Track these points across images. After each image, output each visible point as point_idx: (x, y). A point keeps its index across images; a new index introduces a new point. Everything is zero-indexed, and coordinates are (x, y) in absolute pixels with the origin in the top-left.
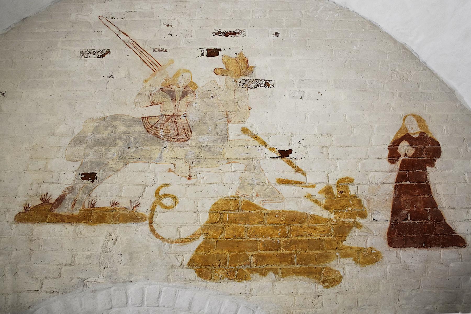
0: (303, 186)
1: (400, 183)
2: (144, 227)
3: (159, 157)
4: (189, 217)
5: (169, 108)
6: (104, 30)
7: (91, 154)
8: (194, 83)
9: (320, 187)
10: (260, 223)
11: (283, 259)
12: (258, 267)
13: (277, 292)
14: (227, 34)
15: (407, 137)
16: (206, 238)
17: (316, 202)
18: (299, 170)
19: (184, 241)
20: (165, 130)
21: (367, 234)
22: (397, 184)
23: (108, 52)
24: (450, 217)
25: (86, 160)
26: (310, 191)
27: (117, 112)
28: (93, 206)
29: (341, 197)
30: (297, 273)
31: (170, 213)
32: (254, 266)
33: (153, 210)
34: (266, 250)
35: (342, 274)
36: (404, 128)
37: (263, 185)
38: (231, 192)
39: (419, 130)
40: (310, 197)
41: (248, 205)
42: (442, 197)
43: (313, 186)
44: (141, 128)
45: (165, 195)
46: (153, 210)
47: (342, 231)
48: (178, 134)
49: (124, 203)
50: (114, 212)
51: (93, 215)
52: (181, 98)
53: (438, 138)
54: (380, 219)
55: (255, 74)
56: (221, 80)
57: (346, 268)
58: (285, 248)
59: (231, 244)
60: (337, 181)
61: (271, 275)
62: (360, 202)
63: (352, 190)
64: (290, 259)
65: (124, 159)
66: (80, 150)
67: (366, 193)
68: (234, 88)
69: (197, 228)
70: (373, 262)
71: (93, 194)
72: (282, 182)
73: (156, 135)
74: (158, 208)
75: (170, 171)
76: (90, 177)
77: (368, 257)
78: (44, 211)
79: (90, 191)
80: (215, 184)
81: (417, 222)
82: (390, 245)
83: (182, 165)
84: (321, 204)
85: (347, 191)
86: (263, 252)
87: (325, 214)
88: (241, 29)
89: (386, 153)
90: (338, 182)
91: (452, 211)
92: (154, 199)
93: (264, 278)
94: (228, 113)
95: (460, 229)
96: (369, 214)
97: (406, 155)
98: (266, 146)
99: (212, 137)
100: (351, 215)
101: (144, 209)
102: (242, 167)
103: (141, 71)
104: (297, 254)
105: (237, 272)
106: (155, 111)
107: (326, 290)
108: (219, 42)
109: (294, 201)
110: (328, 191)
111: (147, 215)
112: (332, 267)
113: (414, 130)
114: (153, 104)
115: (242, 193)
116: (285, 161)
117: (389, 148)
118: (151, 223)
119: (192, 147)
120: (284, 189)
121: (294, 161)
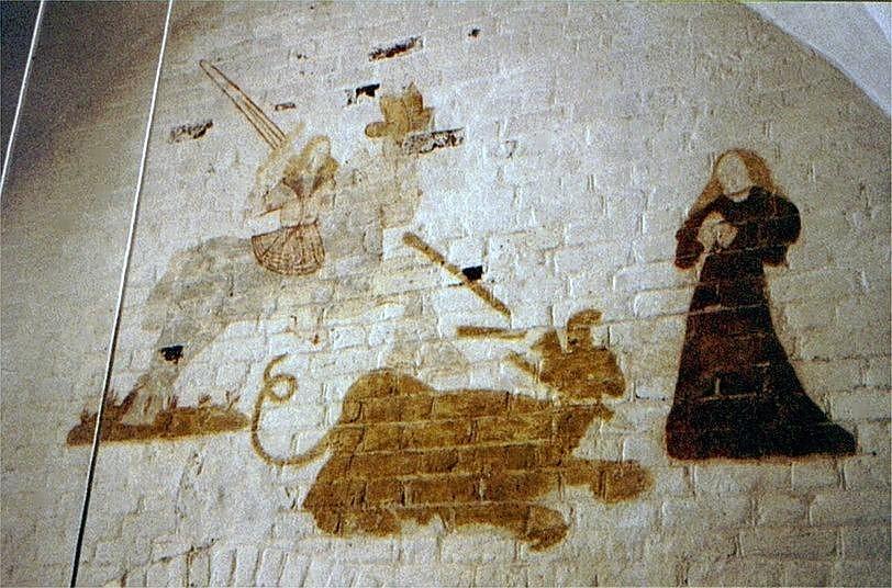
0: (504, 337)
1: (700, 312)
2: (243, 437)
3: (273, 306)
4: (304, 423)
5: (294, 211)
6: (206, 84)
7: (178, 316)
8: (333, 160)
9: (535, 336)
10: (423, 416)
11: (459, 488)
12: (415, 506)
13: (445, 555)
14: (390, 54)
15: (720, 204)
16: (335, 453)
17: (526, 366)
18: (499, 306)
19: (300, 461)
20: (281, 258)
21: (622, 431)
22: (693, 314)
23: (210, 125)
24: (815, 379)
25: (170, 325)
26: (515, 345)
27: (216, 233)
28: (174, 405)
29: (577, 358)
30: (480, 517)
31: (284, 408)
32: (409, 504)
33: (258, 405)
34: (430, 471)
35: (567, 520)
36: (716, 183)
37: (435, 341)
38: (379, 361)
39: (749, 184)
40: (515, 357)
41: (410, 383)
42: (799, 334)
43: (522, 336)
44: (249, 257)
45: (279, 377)
46: (258, 405)
47: (573, 424)
48: (304, 260)
49: (218, 398)
50: (203, 412)
51: (175, 423)
52: (312, 192)
53: (794, 194)
54: (649, 398)
55: (433, 123)
56: (375, 146)
57: (575, 504)
58: (465, 465)
59: (374, 464)
60: (566, 321)
61: (437, 522)
62: (612, 360)
63: (597, 335)
64: (470, 490)
65: (222, 317)
66: (163, 308)
67: (627, 340)
68: (395, 158)
69: (323, 432)
70: (633, 493)
71: (176, 385)
72: (465, 331)
73: (270, 267)
74: (266, 403)
75: (288, 330)
76: (173, 353)
77: (621, 482)
78: (109, 422)
79: (172, 379)
80: (362, 342)
81: (743, 397)
82: (671, 453)
83: (307, 318)
84: (534, 372)
85: (587, 340)
86: (426, 476)
87: (541, 391)
88: (414, 37)
89: (672, 247)
90: (570, 321)
91: (823, 366)
92: (262, 385)
93: (423, 529)
94: (384, 209)
95: (841, 409)
96: (630, 385)
97: (716, 244)
98: (443, 263)
99: (356, 259)
100: (593, 390)
101: (245, 407)
102: (400, 309)
103: (255, 152)
104: (485, 477)
105: (379, 517)
106: (272, 222)
107: (534, 554)
108: (378, 72)
109: (488, 369)
110: (549, 342)
111: (250, 415)
112: (546, 504)
113: (738, 185)
114: (270, 209)
115: (398, 358)
116: (473, 289)
117: (680, 235)
118: (254, 428)
119: (323, 282)
120: (471, 343)
121: (488, 287)
